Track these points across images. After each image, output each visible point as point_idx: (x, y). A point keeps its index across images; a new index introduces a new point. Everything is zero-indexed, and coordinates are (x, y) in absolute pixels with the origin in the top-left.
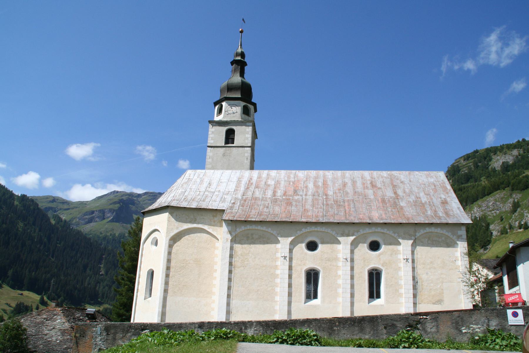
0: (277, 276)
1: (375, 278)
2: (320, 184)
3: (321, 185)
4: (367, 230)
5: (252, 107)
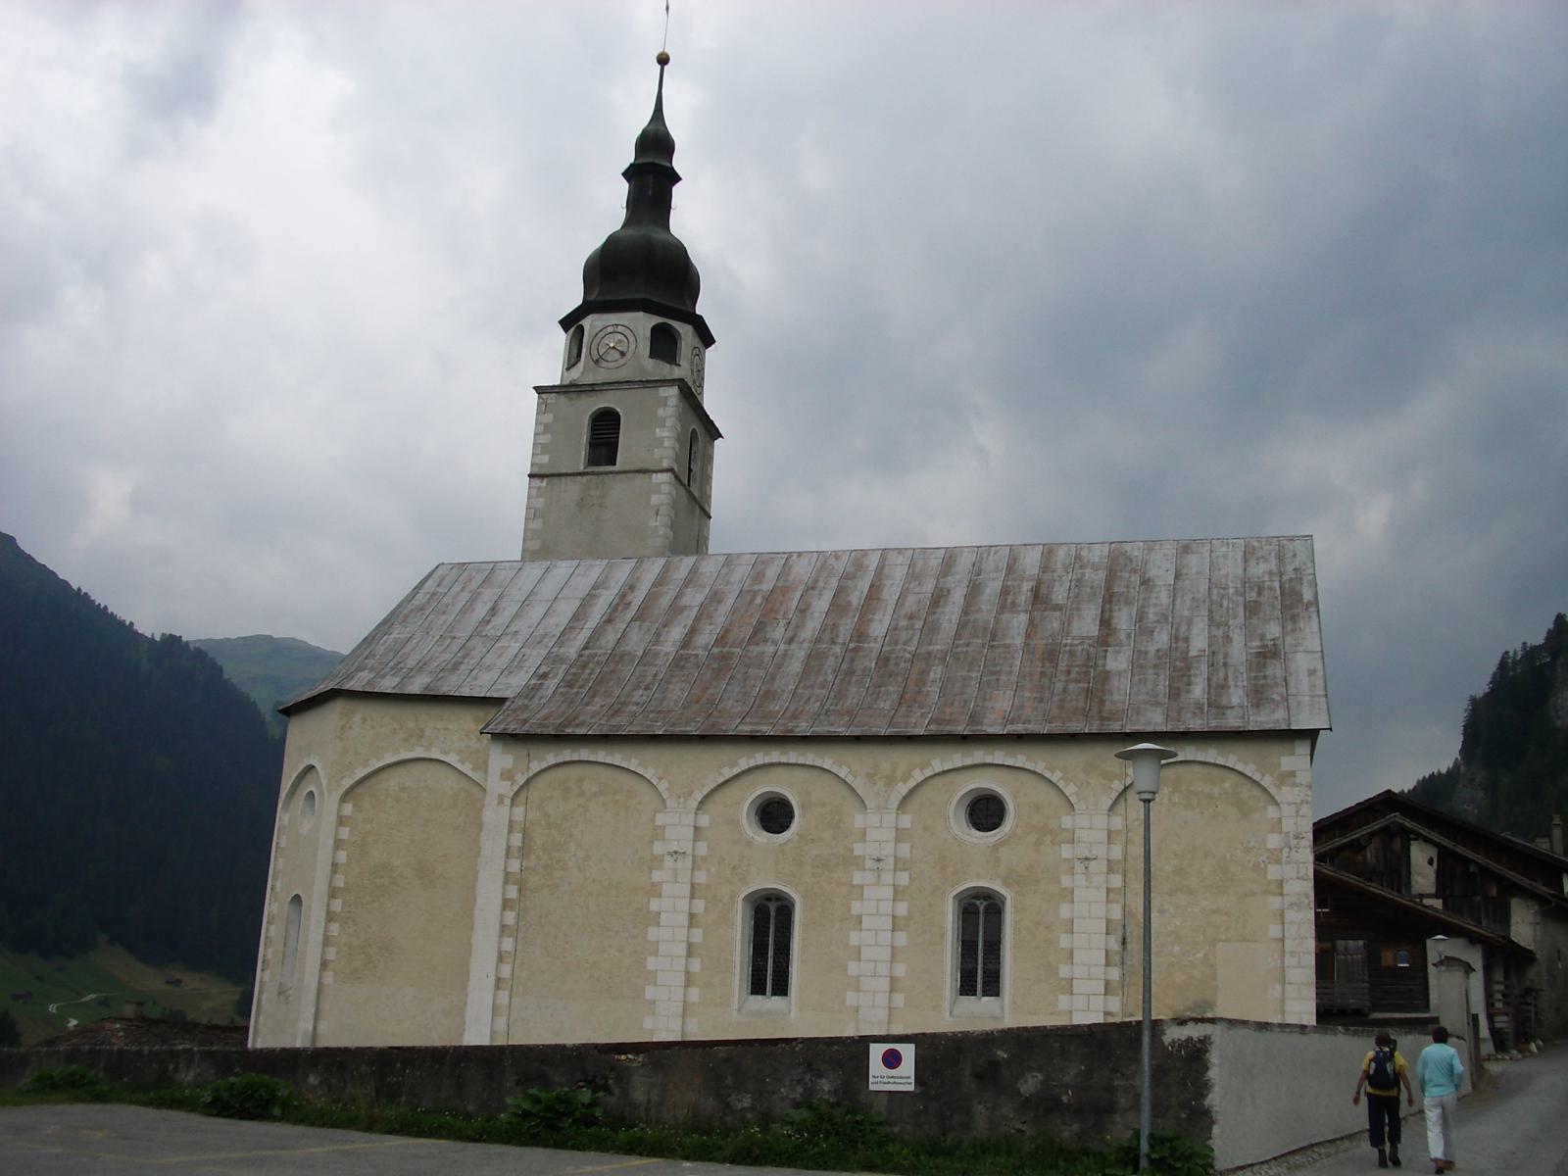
0: (655, 919)
1: (771, 924)
2: (856, 598)
3: (855, 602)
4: (957, 757)
5: (685, 331)
